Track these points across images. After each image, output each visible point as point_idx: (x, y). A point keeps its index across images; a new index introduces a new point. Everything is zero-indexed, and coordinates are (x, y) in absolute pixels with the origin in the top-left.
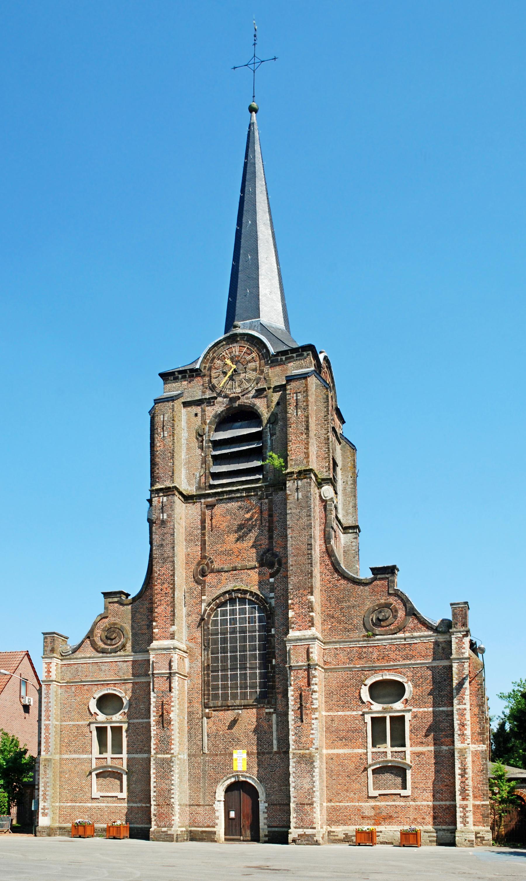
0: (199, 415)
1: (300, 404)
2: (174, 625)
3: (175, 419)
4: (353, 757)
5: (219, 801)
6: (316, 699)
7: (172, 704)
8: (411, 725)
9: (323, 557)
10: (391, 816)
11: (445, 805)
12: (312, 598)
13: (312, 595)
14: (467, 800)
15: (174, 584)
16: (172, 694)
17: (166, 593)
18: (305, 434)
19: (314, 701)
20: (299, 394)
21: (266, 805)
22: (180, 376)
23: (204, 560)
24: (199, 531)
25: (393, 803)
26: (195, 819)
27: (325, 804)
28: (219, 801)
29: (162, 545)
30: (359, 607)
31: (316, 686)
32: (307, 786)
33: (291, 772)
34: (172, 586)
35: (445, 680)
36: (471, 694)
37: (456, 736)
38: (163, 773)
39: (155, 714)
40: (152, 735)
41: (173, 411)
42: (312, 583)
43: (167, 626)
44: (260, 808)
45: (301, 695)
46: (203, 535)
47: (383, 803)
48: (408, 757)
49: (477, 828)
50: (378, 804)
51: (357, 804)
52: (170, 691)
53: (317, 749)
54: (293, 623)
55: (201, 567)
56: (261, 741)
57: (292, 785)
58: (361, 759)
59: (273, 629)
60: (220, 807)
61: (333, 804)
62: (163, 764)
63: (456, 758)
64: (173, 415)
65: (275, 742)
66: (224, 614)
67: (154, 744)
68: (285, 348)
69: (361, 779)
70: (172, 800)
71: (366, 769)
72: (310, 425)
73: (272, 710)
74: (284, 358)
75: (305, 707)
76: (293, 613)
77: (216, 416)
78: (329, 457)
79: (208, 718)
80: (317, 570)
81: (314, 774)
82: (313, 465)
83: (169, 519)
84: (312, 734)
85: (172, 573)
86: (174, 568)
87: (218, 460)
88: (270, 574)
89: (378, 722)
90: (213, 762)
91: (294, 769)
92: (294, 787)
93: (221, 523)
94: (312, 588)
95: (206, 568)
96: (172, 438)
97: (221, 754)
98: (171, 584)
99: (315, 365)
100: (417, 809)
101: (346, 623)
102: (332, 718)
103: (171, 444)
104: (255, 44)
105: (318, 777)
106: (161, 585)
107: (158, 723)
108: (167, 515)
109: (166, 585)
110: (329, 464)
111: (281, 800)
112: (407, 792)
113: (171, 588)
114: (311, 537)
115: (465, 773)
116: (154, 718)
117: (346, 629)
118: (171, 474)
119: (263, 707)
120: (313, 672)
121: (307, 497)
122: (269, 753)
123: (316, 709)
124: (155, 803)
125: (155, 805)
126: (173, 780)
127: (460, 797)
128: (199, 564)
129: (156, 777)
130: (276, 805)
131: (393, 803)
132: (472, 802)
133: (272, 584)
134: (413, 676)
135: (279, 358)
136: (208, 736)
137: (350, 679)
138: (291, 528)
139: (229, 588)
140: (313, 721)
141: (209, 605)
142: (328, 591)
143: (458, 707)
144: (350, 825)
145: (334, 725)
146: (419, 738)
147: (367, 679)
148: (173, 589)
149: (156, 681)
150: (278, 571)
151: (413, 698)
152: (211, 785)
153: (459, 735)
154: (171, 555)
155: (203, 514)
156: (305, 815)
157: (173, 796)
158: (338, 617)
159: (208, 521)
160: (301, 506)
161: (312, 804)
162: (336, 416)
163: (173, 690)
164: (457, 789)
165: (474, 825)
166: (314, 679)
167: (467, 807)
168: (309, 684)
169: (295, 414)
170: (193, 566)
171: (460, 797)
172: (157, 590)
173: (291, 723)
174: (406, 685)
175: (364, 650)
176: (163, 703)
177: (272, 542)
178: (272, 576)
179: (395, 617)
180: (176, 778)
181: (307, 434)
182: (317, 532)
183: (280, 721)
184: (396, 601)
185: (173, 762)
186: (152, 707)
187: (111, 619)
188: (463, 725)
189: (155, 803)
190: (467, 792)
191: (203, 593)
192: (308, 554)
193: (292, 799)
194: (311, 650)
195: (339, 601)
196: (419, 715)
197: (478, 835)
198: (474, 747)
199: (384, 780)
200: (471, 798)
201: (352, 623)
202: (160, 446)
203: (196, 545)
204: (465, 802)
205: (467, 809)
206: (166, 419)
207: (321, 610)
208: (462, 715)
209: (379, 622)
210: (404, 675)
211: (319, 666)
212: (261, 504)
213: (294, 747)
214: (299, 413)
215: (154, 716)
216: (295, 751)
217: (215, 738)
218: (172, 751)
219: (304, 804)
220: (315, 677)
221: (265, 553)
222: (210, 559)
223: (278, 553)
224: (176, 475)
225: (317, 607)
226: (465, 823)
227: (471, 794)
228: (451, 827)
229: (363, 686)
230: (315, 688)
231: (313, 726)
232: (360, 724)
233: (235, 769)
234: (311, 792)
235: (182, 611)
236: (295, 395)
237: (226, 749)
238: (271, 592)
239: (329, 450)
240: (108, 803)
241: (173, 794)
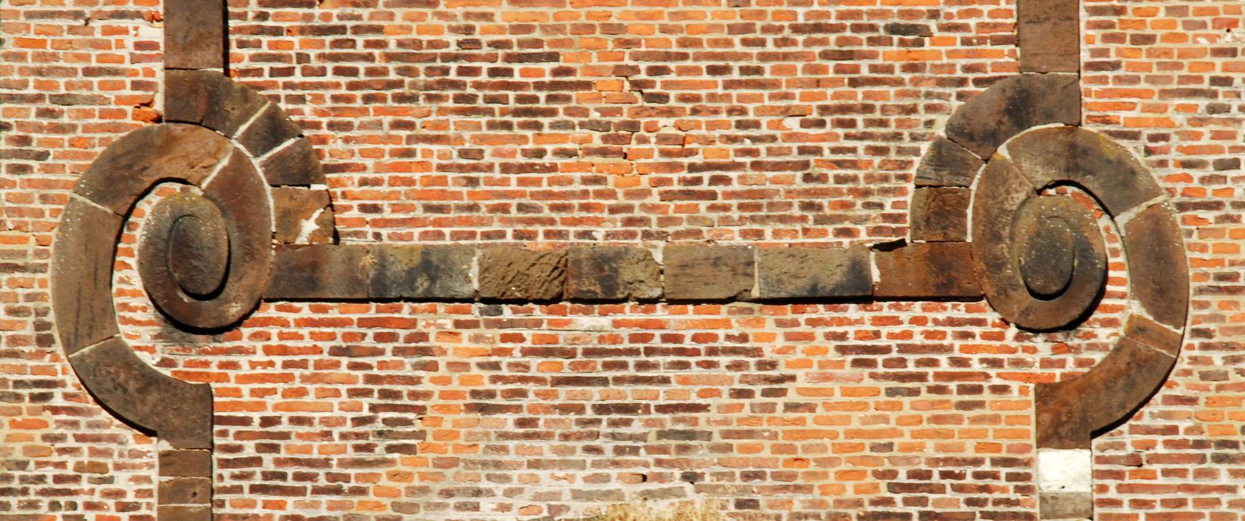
87: (1027, 464)
150: (1139, 375)
178: (1072, 416)
222: (275, 128)
223: (1134, 151)
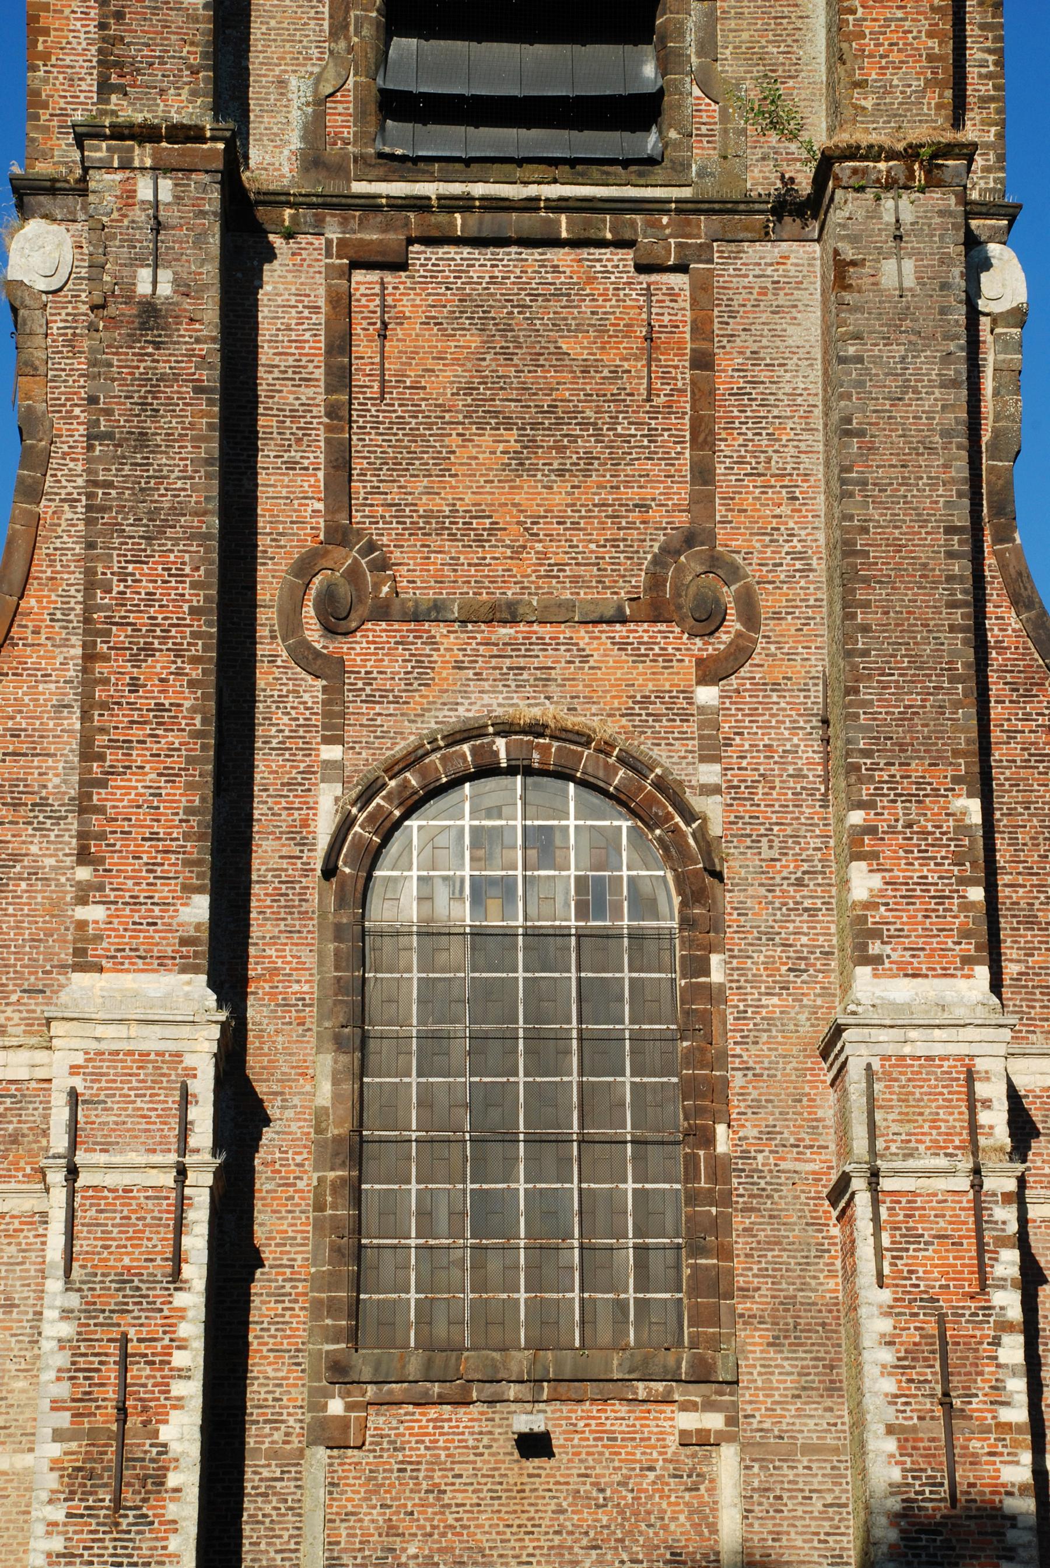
23: (339, 552)
29: (142, 439)
59: (715, 959)
73: (715, 1421)
75: (963, 1415)
76: (876, 881)
83: (187, 304)
93: (430, 363)
106: (135, 661)
107: (78, 1479)
109: (160, 664)
116: (55, 1450)
119: (667, 1400)
133: (710, 719)
139: (468, 711)
155: (342, 305)
159: (364, 348)
172: (106, 681)
177: (710, 499)
178: (711, 672)
221: (668, 553)
223: (738, 559)
238: (703, 759)
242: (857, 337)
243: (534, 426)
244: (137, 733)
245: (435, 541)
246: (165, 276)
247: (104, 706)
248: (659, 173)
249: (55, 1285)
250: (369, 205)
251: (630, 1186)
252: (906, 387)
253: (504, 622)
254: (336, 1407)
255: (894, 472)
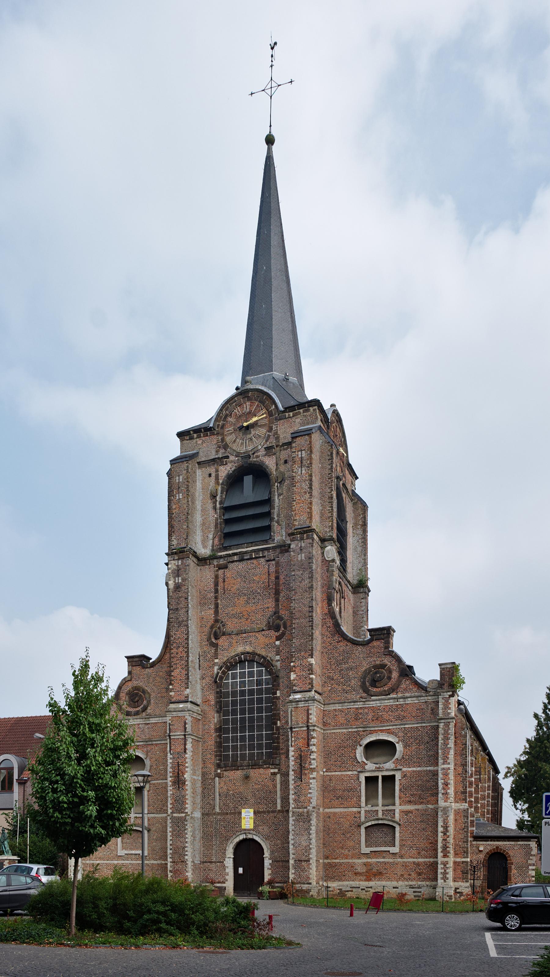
0: (213, 475)
1: (304, 462)
2: (188, 688)
3: (189, 480)
4: (348, 815)
5: (229, 858)
6: (314, 759)
7: (187, 765)
8: (401, 784)
9: (325, 619)
10: (381, 873)
11: (429, 862)
12: (312, 661)
13: (312, 657)
14: (448, 857)
15: (188, 648)
16: (186, 756)
17: (181, 657)
18: (309, 493)
19: (312, 762)
20: (303, 452)
21: (271, 861)
22: (195, 435)
23: (217, 624)
24: (212, 594)
25: (382, 860)
26: (208, 875)
27: (321, 861)
28: (229, 858)
29: (177, 609)
30: (356, 669)
31: (314, 747)
32: (304, 844)
33: (291, 830)
34: (186, 650)
35: (432, 740)
36: (456, 754)
37: (440, 795)
38: (179, 831)
39: (171, 774)
40: (169, 795)
41: (187, 472)
42: (312, 645)
43: (182, 689)
44: (265, 864)
45: (301, 756)
46: (216, 598)
47: (374, 860)
48: (397, 815)
49: (457, 884)
50: (369, 860)
51: (350, 861)
52: (185, 752)
53: (314, 808)
54: (294, 685)
55: (214, 630)
56: (266, 800)
57: (291, 842)
58: (355, 817)
59: (278, 692)
60: (229, 863)
61: (329, 861)
62: (178, 823)
63: (439, 816)
64: (187, 477)
65: (279, 801)
66: (234, 677)
67: (171, 804)
68: (292, 403)
69: (355, 836)
70: (186, 857)
71: (359, 826)
72: (313, 484)
73: (276, 770)
74: (291, 414)
75: (304, 767)
76: (295, 676)
77: (229, 476)
78: (332, 517)
79: (219, 777)
80: (317, 634)
81: (311, 832)
82: (316, 524)
84: (310, 793)
85: (186, 637)
86: (188, 632)
87: (228, 522)
88: (276, 637)
89: (371, 781)
90: (224, 820)
91: (293, 827)
92: (293, 845)
94: (312, 650)
95: (218, 631)
96: (186, 500)
97: (231, 813)
98: (186, 648)
99: (321, 420)
100: (405, 865)
101: (345, 685)
102: (330, 778)
103: (185, 506)
104: (272, 66)
105: (314, 835)
106: (177, 649)
107: (174, 783)
108: (182, 579)
110: (332, 524)
111: (283, 857)
112: (395, 850)
113: (186, 652)
114: (312, 600)
115: (447, 831)
116: (170, 779)
117: (344, 690)
118: (185, 537)
120: (312, 733)
121: (310, 558)
122: (273, 812)
123: (314, 768)
124: (171, 860)
125: (171, 862)
126: (187, 838)
127: (442, 854)
128: (212, 627)
129: (172, 835)
130: (279, 861)
131: (382, 860)
132: (452, 859)
133: (278, 647)
134: (404, 737)
135: (287, 414)
136: (220, 795)
137: (347, 740)
138: (294, 590)
140: (311, 781)
141: (221, 668)
142: (327, 652)
143: (443, 766)
144: (344, 881)
145: (332, 785)
146: (408, 797)
147: (362, 739)
148: (187, 652)
149: (173, 743)
150: (283, 634)
151: (403, 758)
152: (221, 843)
153: (443, 794)
154: (185, 619)
155: (217, 577)
156: (302, 871)
157: (187, 853)
158: (337, 679)
160: (304, 568)
161: (309, 861)
162: (347, 472)
163: (187, 751)
164: (439, 847)
165: (455, 881)
166: (312, 740)
167: (448, 864)
168: (308, 745)
169: (299, 473)
170: (207, 629)
171: (442, 854)
173: (291, 782)
174: (397, 745)
175: (360, 711)
176: (178, 764)
178: (278, 638)
179: (390, 678)
180: (189, 836)
181: (311, 493)
182: (318, 594)
183: (284, 781)
184: (390, 662)
185: (187, 821)
186: (169, 768)
187: (135, 683)
188: (446, 784)
189: (171, 860)
190: (448, 849)
191: (216, 656)
192: (309, 617)
193: (291, 856)
194: (310, 712)
195: (339, 663)
196: (408, 775)
197: (458, 891)
198: (455, 806)
199: (376, 838)
200: (451, 855)
201: (349, 685)
202: (175, 509)
203: (210, 608)
204: (446, 859)
205: (447, 866)
206: (181, 480)
207: (323, 672)
208: (446, 774)
209: (374, 683)
210: (396, 735)
211: (318, 727)
212: (269, 566)
213: (293, 806)
214: (304, 472)
215: (171, 777)
216: (294, 810)
217: (226, 797)
218: (186, 811)
219: (302, 861)
220: (313, 738)
222: (222, 622)
224: (190, 538)
225: (317, 669)
226: (445, 879)
227: (452, 852)
228: (434, 883)
229: (358, 747)
230: (314, 748)
231: (311, 786)
232: (270, 784)
233: (243, 827)
234: (308, 849)
235: (195, 675)
236: (300, 453)
237: (235, 808)
239: (332, 509)
240: (132, 860)
241: (187, 851)
242: (294, 570)
243: (249, 595)
244: (178, 662)
245: (233, 619)
246: (180, 578)
247: (173, 658)
248: (270, 541)
249: (169, 754)
250: (221, 557)
251: (264, 733)
252: (302, 580)
253: (244, 633)
254: (219, 771)
255: (300, 597)
